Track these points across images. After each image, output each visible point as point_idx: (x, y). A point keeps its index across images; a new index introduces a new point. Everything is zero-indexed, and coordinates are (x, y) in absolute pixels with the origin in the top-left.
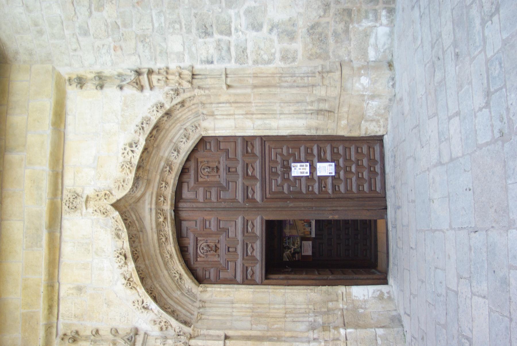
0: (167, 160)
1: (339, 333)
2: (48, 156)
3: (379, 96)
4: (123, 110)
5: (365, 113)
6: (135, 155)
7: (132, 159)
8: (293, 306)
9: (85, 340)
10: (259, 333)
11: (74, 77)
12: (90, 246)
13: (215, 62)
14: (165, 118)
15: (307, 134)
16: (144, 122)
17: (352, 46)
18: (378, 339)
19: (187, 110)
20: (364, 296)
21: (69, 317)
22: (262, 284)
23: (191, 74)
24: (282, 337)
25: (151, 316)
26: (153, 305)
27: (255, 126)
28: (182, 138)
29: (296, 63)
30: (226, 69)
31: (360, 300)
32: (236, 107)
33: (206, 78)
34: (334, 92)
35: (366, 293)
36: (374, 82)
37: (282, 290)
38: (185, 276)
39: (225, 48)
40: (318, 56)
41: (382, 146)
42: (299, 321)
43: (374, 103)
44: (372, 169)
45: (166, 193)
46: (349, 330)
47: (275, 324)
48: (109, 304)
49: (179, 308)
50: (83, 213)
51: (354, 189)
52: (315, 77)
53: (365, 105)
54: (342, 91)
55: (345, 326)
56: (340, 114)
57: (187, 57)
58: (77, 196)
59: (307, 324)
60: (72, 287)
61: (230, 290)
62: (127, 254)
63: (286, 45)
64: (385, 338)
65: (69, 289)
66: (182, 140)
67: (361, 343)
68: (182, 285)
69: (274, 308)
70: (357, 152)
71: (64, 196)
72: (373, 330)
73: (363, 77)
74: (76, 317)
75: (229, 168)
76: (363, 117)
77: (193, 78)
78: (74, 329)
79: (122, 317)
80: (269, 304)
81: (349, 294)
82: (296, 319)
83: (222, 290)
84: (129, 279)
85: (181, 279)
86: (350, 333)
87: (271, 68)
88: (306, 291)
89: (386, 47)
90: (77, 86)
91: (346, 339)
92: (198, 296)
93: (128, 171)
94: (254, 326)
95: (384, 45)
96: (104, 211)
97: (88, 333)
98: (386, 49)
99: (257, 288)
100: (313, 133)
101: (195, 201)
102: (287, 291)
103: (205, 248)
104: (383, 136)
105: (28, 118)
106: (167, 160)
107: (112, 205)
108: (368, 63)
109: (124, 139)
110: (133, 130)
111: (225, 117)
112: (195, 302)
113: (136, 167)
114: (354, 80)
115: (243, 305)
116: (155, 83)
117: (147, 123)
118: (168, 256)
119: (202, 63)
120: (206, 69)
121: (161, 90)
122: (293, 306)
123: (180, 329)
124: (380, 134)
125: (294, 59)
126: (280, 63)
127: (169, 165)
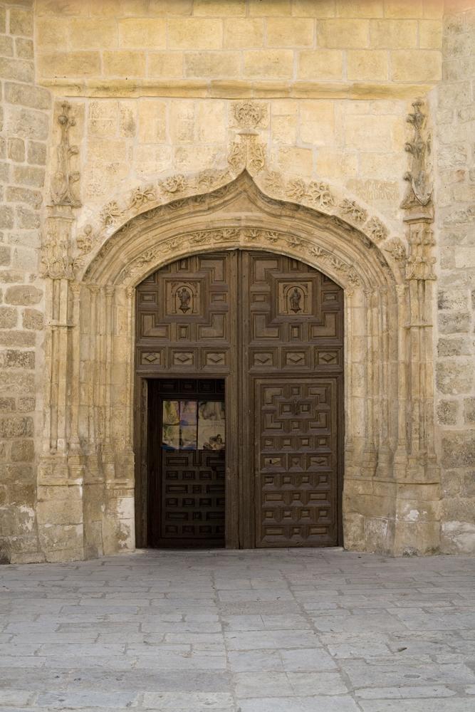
0: (309, 242)
1: (78, 477)
2: (313, 81)
3: (393, 536)
4: (376, 182)
5: (373, 518)
6: (314, 201)
7: (308, 198)
8: (108, 417)
9: (63, 138)
10: (76, 371)
11: (423, 111)
12: (189, 141)
13: (440, 311)
14: (365, 241)
15: (346, 438)
16: (359, 214)
17: (461, 499)
18: (71, 527)
19: (378, 270)
20: (122, 513)
21: (93, 113)
22: (137, 374)
23: (425, 277)
24: (72, 402)
25: (97, 224)
26: (111, 230)
27: (356, 364)
28: (339, 264)
29: (438, 422)
30: (432, 326)
31: (115, 508)
32: (382, 339)
33: (418, 300)
34: (400, 473)
35: (126, 515)
36: (412, 528)
37: (129, 401)
38: (147, 268)
39: (459, 326)
40: (447, 453)
41: (329, 545)
42: (89, 425)
43: (385, 531)
44: (296, 530)
45: (262, 239)
46: (81, 489)
47: (85, 393)
48: (112, 169)
49: (105, 263)
50: (233, 130)
51: (268, 504)
52: (420, 448)
53: (383, 518)
54: (400, 485)
55: (85, 485)
56: (371, 483)
57: (448, 272)
58: (257, 120)
59: (86, 435)
60: (133, 116)
61: (129, 331)
62: (179, 193)
63: (462, 409)
64: (71, 535)
65: (131, 112)
66: (337, 261)
67: (65, 504)
68: (134, 264)
69: (105, 391)
70: (320, 509)
71: (256, 101)
72: (81, 521)
73: (418, 513)
74: (93, 123)
75: (298, 327)
76: (368, 515)
77: (418, 280)
78: (77, 120)
79: (94, 188)
80: (111, 384)
81: (124, 493)
82: (92, 421)
83: (129, 319)
84: (146, 197)
85: (144, 262)
86: (78, 491)
87: (432, 388)
88: (128, 434)
89: (460, 545)
90: (411, 115)
91: (69, 486)
92: (121, 286)
93: (292, 193)
94: (83, 364)
95: (462, 543)
96: (237, 160)
97: (72, 141)
98: (456, 546)
99: (131, 368)
100: (347, 446)
101: (252, 280)
102: (128, 408)
103: (185, 294)
104: (343, 546)
105: (365, 49)
106: (309, 242)
107: (245, 170)
108: (439, 521)
109: (337, 185)
110: (348, 198)
111: (369, 323)
112: (113, 282)
113: (297, 203)
114: (414, 501)
115: (109, 350)
116: (414, 227)
117: (357, 217)
118: (175, 245)
119: (440, 293)
120: (432, 299)
121: (404, 235)
122: (108, 417)
123: (80, 267)
124: (346, 542)
125: (443, 420)
126: (439, 400)
127: (303, 243)
